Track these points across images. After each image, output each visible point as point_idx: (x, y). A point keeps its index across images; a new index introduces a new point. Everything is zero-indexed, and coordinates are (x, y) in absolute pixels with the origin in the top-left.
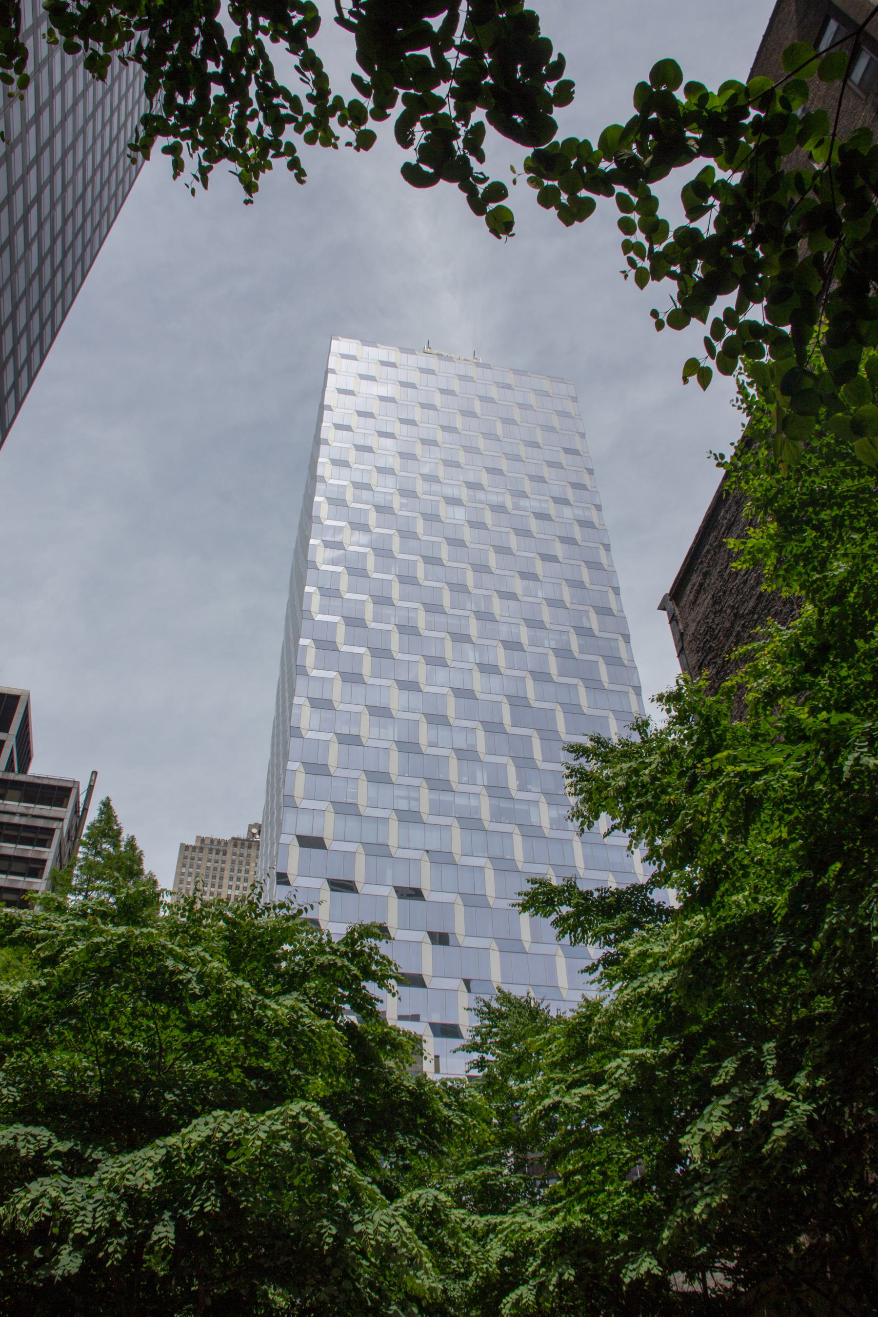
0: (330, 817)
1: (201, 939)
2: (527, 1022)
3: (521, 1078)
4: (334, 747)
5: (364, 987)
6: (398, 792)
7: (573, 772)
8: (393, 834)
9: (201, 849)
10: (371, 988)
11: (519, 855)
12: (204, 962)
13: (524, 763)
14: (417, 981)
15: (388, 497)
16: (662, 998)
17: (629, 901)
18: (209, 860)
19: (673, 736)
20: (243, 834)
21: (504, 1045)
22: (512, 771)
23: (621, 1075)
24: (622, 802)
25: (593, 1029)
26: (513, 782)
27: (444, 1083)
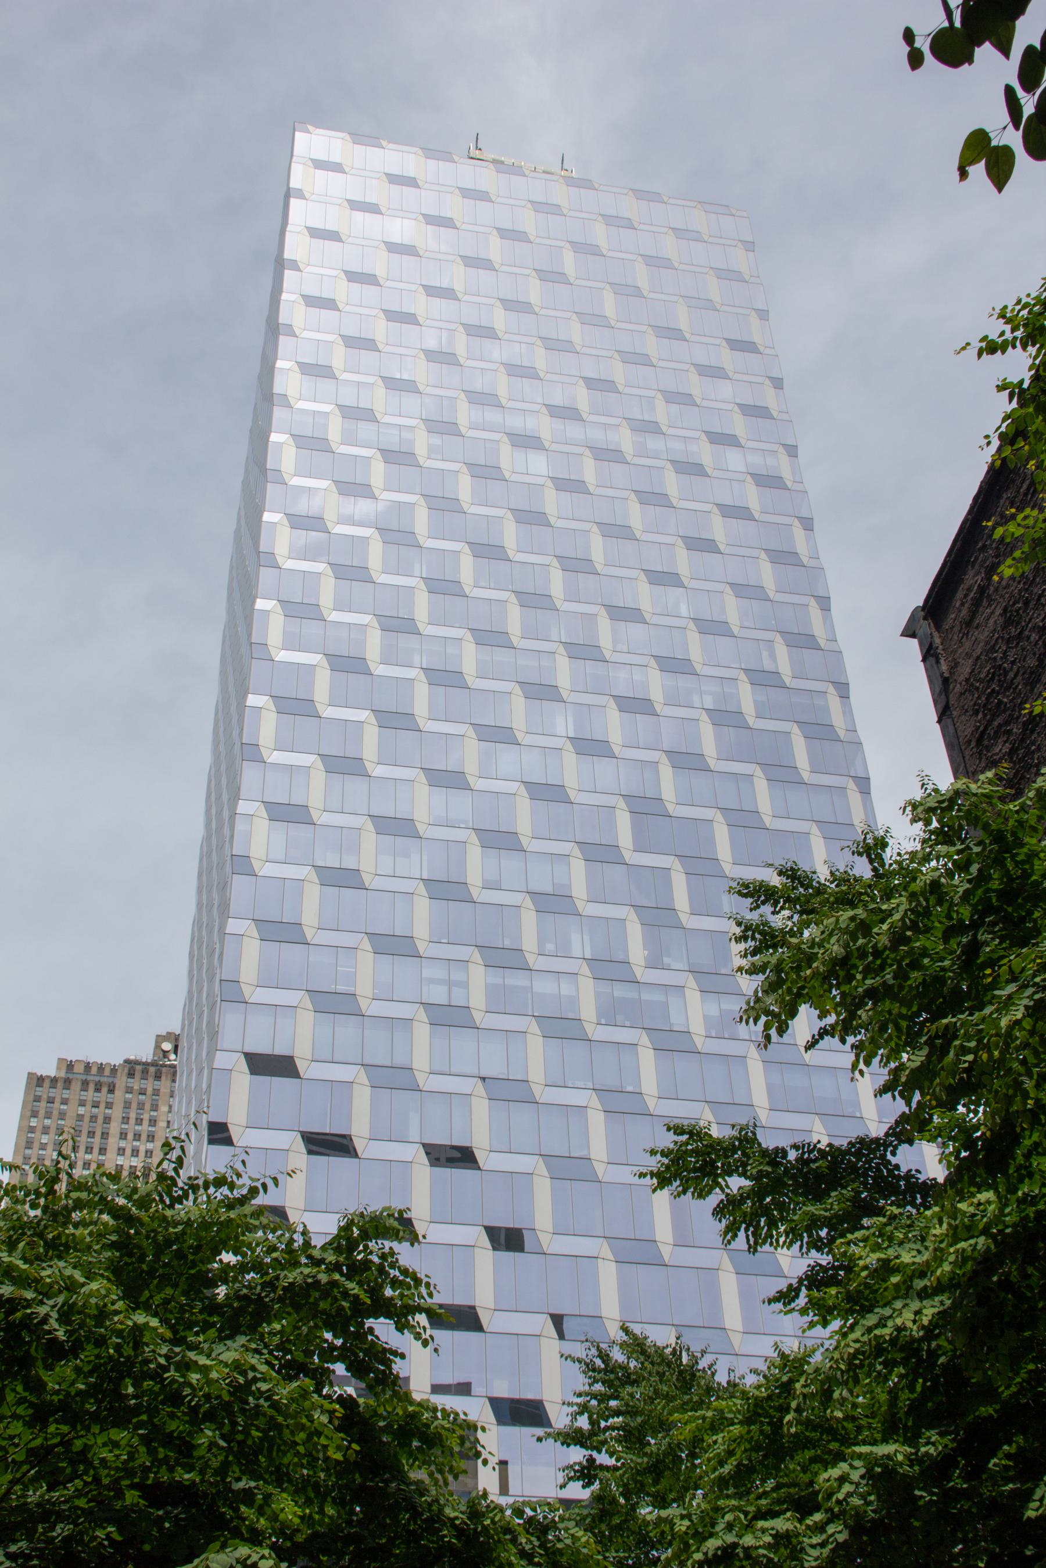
0: (307, 1018)
1: (67, 1247)
2: (674, 1392)
3: (661, 1502)
4: (313, 892)
5: (371, 1330)
6: (430, 971)
7: (748, 930)
8: (421, 1048)
9: (67, 1082)
10: (383, 1329)
11: (649, 1085)
12: (71, 1287)
13: (658, 917)
14: (465, 1319)
15: (406, 435)
16: (919, 1350)
17: (854, 1168)
18: (82, 1103)
19: (933, 863)
20: (146, 1054)
21: (633, 1438)
22: (635, 931)
23: (849, 1494)
24: (838, 986)
25: (794, 1404)
26: (637, 953)
27: (518, 1512)
